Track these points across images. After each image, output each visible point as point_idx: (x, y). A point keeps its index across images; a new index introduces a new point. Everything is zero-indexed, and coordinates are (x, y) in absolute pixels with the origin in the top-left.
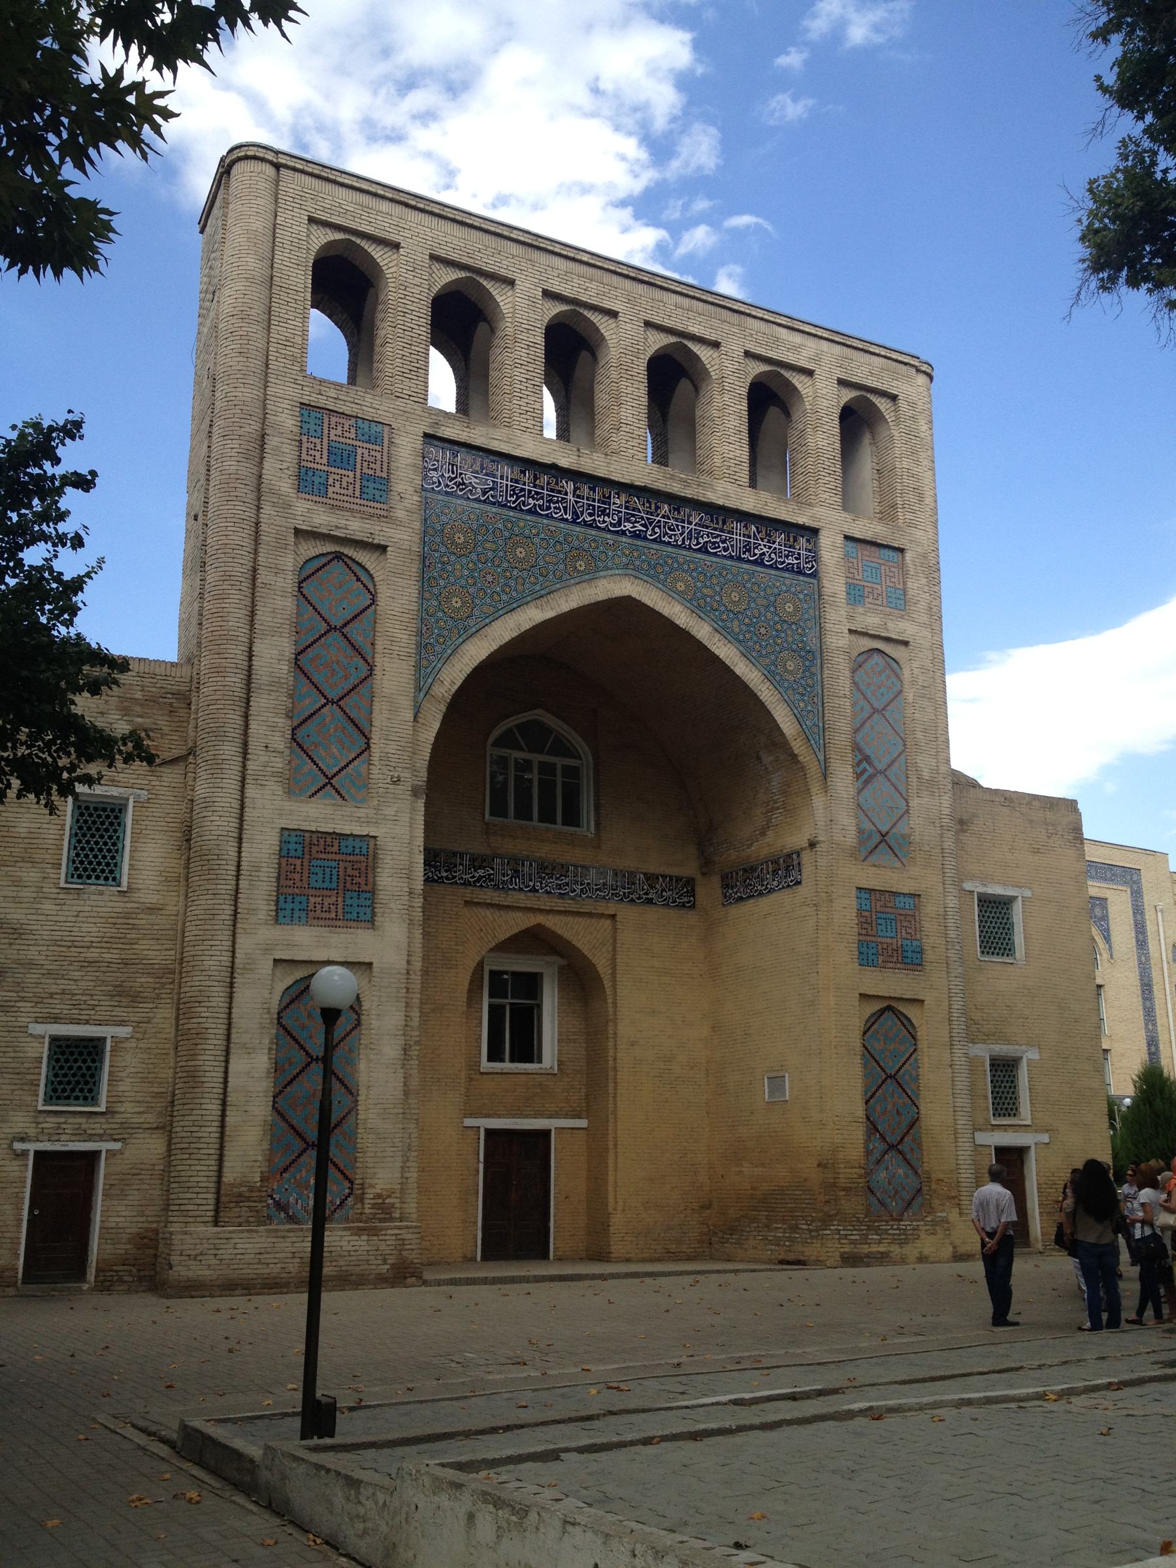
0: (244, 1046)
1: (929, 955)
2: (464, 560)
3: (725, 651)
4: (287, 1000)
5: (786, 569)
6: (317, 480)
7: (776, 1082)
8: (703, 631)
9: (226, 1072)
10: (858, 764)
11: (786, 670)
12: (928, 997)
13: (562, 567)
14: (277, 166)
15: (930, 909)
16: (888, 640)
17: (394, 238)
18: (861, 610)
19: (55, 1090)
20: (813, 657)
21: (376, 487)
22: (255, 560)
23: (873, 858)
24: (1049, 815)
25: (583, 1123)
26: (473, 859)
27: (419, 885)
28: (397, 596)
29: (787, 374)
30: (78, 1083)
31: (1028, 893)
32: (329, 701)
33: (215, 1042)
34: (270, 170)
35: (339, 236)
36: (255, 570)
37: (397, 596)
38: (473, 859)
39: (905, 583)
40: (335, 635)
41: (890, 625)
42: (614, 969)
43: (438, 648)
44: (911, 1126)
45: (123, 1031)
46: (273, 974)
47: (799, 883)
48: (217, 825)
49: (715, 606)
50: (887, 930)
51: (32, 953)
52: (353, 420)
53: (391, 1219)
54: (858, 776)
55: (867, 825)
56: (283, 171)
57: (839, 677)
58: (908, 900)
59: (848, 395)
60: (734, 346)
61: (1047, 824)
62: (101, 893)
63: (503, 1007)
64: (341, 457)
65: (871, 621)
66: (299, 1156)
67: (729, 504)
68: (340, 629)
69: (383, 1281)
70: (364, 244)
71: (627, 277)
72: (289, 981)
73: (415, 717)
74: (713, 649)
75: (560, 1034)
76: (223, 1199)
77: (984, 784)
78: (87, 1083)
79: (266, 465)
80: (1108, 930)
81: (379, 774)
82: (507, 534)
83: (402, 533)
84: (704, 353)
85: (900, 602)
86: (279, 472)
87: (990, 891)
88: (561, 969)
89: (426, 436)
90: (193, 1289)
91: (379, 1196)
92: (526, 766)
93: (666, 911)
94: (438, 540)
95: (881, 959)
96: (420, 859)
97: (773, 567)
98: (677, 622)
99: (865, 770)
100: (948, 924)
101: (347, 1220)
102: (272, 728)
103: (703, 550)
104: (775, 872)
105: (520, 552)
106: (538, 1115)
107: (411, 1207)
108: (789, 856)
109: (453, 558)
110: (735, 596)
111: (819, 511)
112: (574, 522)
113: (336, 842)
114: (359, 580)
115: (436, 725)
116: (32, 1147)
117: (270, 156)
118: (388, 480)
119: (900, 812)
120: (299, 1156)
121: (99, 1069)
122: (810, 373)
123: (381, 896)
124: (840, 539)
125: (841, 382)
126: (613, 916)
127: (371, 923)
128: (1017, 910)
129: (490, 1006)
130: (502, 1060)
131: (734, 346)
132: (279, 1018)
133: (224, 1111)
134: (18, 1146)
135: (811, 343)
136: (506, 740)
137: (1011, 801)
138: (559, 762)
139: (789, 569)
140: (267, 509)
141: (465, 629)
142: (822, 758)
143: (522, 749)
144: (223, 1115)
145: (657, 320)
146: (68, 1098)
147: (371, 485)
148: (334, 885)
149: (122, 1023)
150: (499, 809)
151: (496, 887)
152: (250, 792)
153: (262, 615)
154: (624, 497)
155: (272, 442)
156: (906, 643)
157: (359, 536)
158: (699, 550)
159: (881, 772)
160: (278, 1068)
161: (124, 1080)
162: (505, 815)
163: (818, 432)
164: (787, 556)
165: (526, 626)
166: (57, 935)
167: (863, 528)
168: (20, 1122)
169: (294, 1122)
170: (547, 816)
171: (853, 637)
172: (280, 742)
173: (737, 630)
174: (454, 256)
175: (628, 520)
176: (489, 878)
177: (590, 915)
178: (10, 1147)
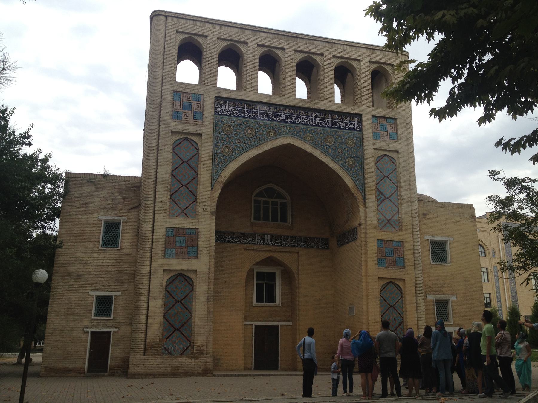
0: (154, 298)
1: (407, 263)
2: (229, 136)
3: (325, 159)
4: (168, 283)
5: (349, 129)
6: (178, 115)
7: (351, 309)
8: (317, 153)
9: (148, 306)
10: (378, 196)
11: (349, 164)
12: (406, 277)
13: (264, 135)
14: (166, 16)
15: (407, 246)
16: (390, 151)
17: (205, 34)
18: (379, 141)
19: (98, 312)
20: (361, 159)
21: (199, 116)
22: (158, 142)
23: (385, 229)
24: (461, 210)
25: (290, 323)
26: (247, 235)
27: (213, 243)
28: (206, 150)
29: (350, 62)
30: (105, 310)
31: (452, 239)
32: (183, 186)
33: (144, 296)
34: (164, 18)
35: (187, 36)
36: (158, 145)
37: (206, 150)
38: (247, 235)
39: (397, 130)
40: (185, 164)
41: (390, 146)
42: (298, 270)
43: (220, 166)
44: (400, 325)
45: (118, 293)
46: (164, 274)
47: (357, 239)
48: (147, 227)
49: (322, 144)
50: (391, 254)
51: (91, 269)
52: (191, 95)
53: (203, 354)
54: (378, 200)
55: (381, 217)
56: (168, 17)
57: (370, 166)
58: (398, 243)
59: (374, 66)
60: (329, 55)
61: (460, 214)
62: (112, 250)
63: (263, 284)
64: (187, 107)
65: (382, 144)
66: (172, 333)
67: (326, 109)
68: (187, 162)
69: (199, 375)
70: (196, 37)
71: (288, 36)
72: (169, 276)
73: (212, 189)
74: (321, 159)
75: (282, 293)
76: (147, 347)
77: (439, 200)
78: (108, 310)
79: (162, 112)
81: (200, 208)
82: (245, 126)
83: (207, 129)
85: (395, 137)
86: (166, 115)
87: (436, 239)
88: (282, 271)
89: (216, 97)
90: (136, 376)
91: (199, 346)
92: (274, 203)
94: (220, 130)
95: (387, 264)
96: (213, 236)
97: (345, 129)
98: (308, 151)
99: (381, 198)
100: (418, 250)
101: (188, 354)
102: (163, 195)
103: (317, 125)
104: (350, 235)
106: (274, 321)
107: (210, 350)
108: (354, 229)
109: (226, 136)
110: (329, 140)
111: (362, 108)
113: (185, 231)
114: (193, 145)
115: (220, 191)
116: (90, 330)
117: (163, 13)
118: (203, 112)
119: (395, 212)
120: (172, 333)
121: (111, 305)
122: (359, 60)
123: (200, 248)
124: (370, 117)
125: (370, 62)
126: (298, 253)
127: (196, 257)
128: (448, 244)
129: (257, 284)
130: (263, 302)
131: (329, 55)
132: (166, 288)
133: (147, 318)
134: (86, 330)
135: (359, 50)
136: (260, 194)
137: (445, 206)
138: (279, 201)
139: (351, 129)
140: (162, 126)
141: (230, 159)
142: (363, 194)
143: (265, 197)
144: (147, 320)
145: (299, 49)
146: (102, 315)
147: (197, 115)
148: (184, 245)
149: (118, 291)
150: (257, 218)
151: (255, 244)
152: (156, 216)
154: (287, 110)
155: (163, 104)
156: (397, 152)
157: (192, 131)
158: (316, 126)
159: (387, 198)
160: (165, 304)
161: (118, 308)
162: (260, 220)
163: (364, 81)
164: (350, 125)
165: (251, 156)
166: (98, 264)
167: (380, 112)
168: (86, 322)
169: (171, 322)
170: (275, 219)
171: (376, 151)
172: (167, 199)
173: (330, 152)
174: (226, 37)
175: (289, 118)
176: (253, 241)
177: (290, 252)
178: (83, 330)
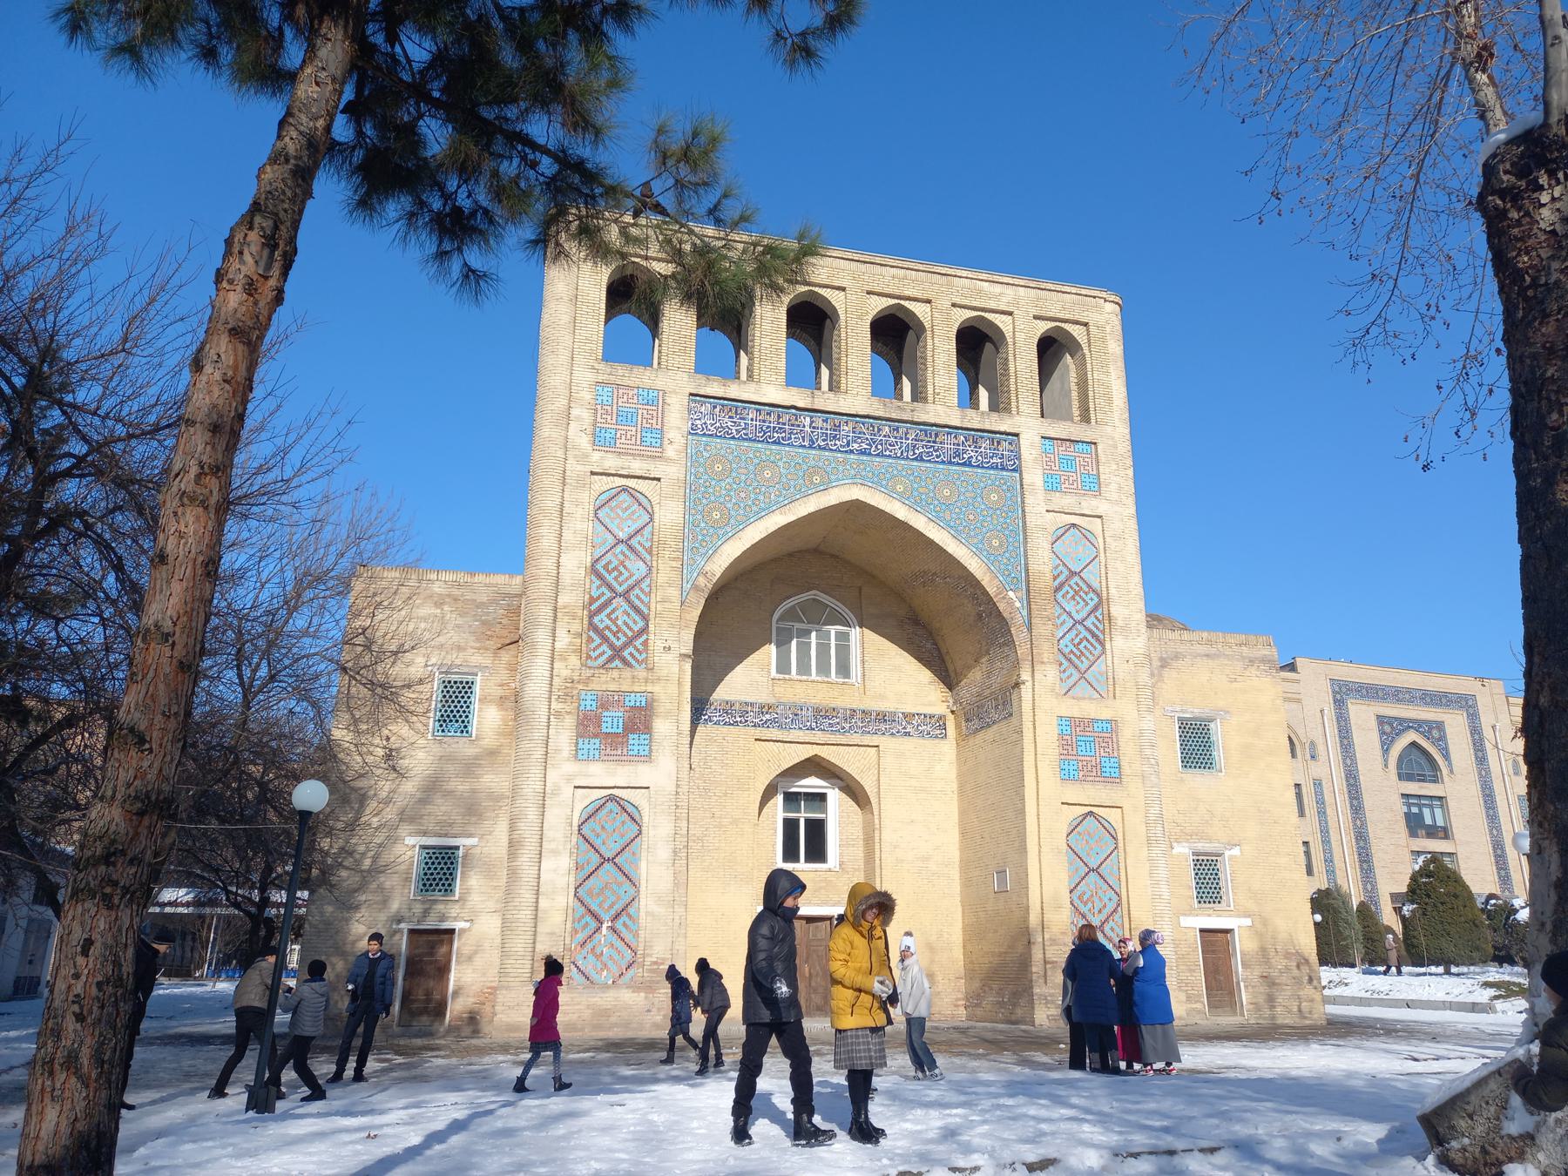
4: (585, 816)
32: (617, 595)
80: (1446, 749)
84: (999, 320)
93: (921, 741)
103: (920, 459)
105: (767, 474)
110: (946, 492)
112: (811, 447)
139: (994, 467)
153: (567, 535)
155: (575, 412)
176: (774, 721)
